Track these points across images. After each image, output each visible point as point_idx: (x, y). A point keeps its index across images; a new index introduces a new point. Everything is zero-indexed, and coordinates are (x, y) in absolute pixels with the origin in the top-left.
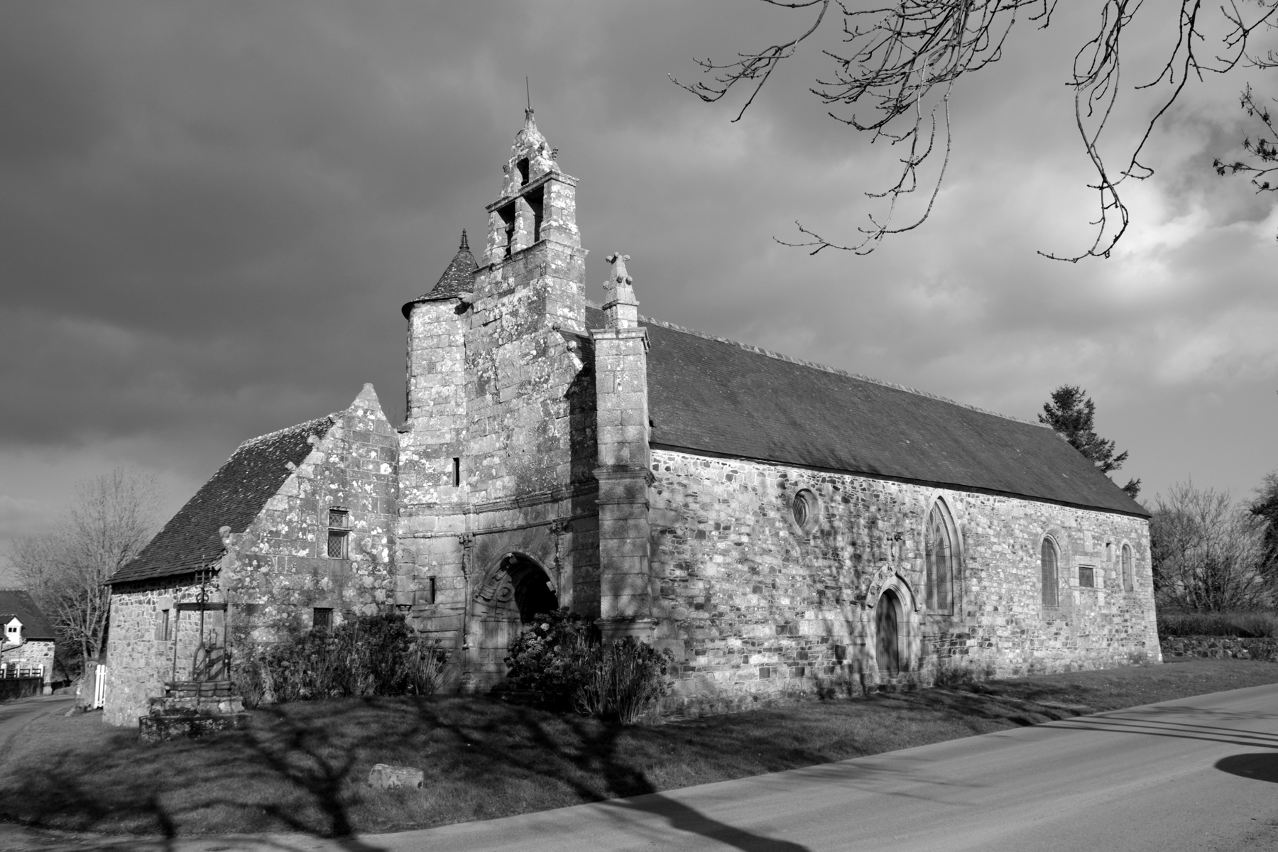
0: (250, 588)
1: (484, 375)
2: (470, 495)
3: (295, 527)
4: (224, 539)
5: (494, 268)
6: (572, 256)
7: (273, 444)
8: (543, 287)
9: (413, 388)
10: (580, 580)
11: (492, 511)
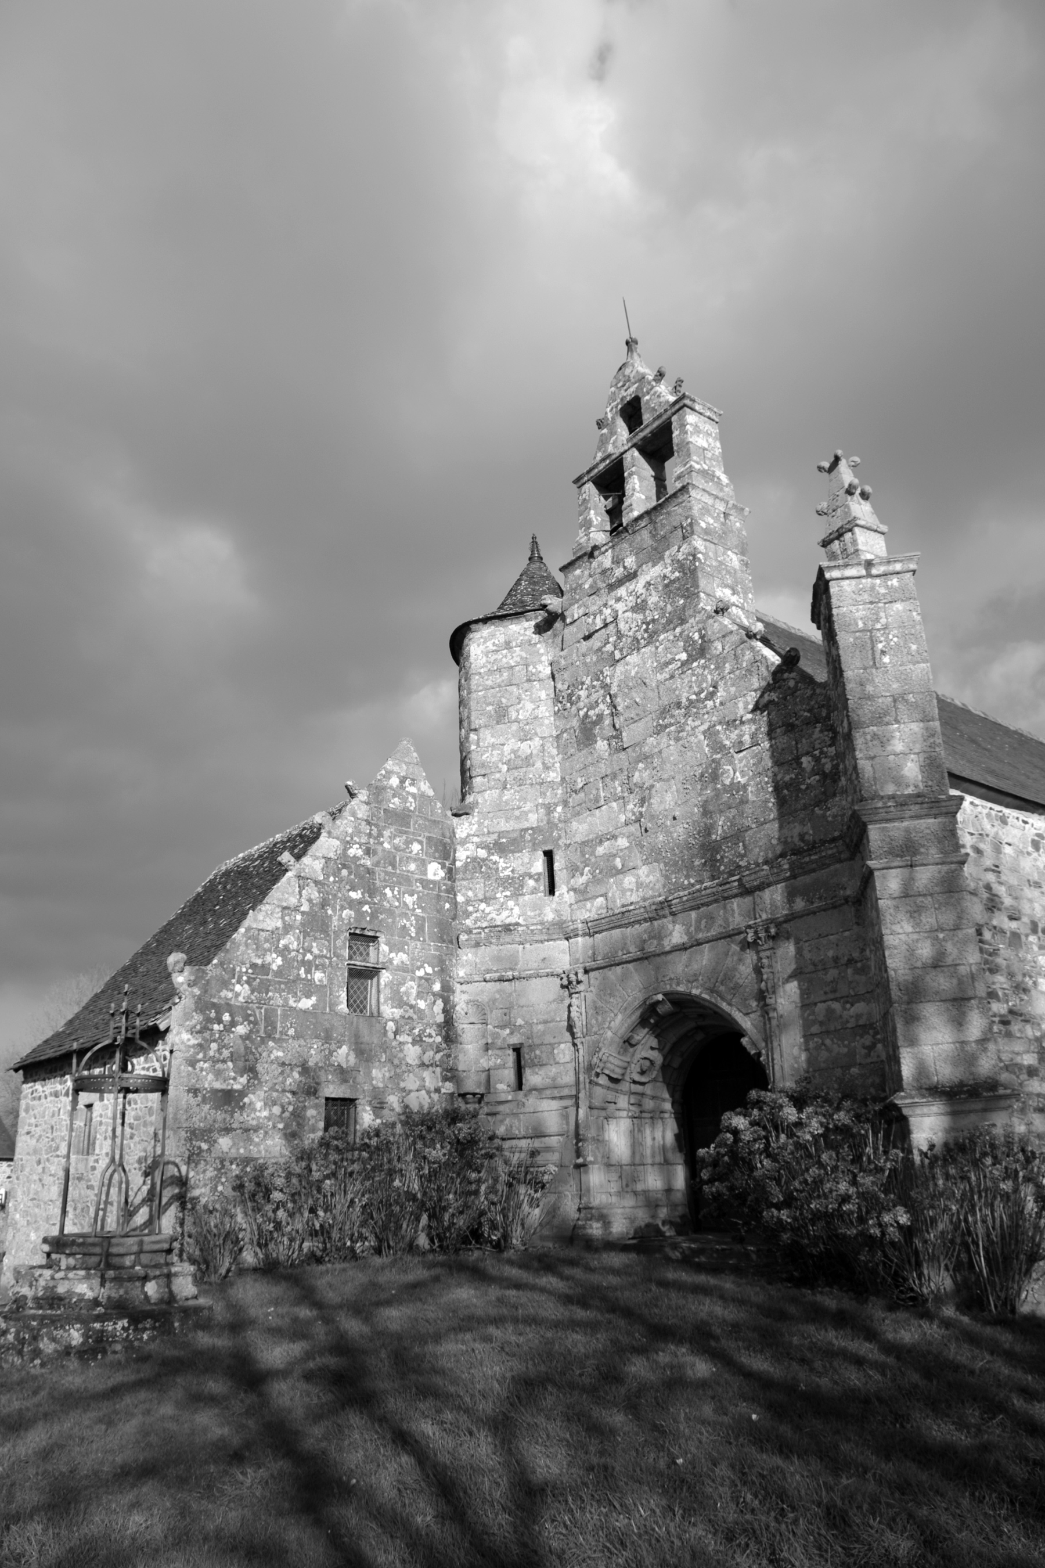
0: (218, 1061)
1: (591, 713)
2: (575, 907)
3: (294, 959)
4: (174, 975)
5: (596, 553)
6: (726, 515)
7: (260, 856)
8: (689, 554)
9: (473, 747)
10: (815, 1029)
11: (620, 926)
